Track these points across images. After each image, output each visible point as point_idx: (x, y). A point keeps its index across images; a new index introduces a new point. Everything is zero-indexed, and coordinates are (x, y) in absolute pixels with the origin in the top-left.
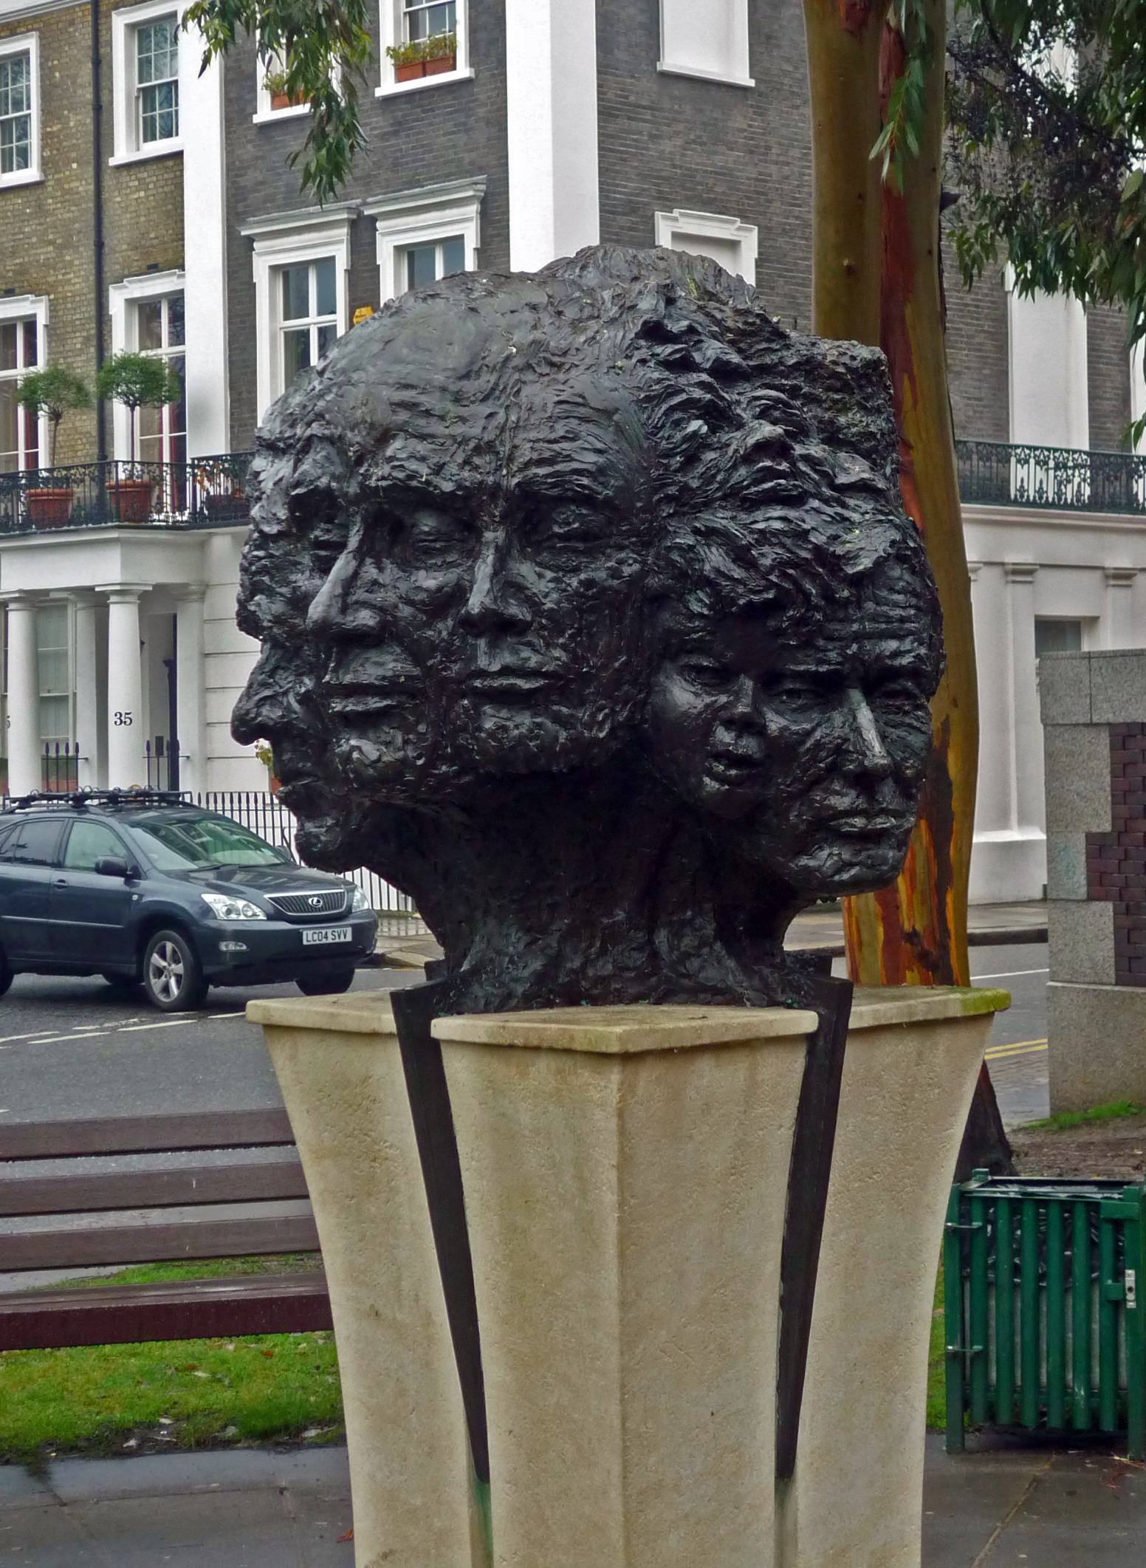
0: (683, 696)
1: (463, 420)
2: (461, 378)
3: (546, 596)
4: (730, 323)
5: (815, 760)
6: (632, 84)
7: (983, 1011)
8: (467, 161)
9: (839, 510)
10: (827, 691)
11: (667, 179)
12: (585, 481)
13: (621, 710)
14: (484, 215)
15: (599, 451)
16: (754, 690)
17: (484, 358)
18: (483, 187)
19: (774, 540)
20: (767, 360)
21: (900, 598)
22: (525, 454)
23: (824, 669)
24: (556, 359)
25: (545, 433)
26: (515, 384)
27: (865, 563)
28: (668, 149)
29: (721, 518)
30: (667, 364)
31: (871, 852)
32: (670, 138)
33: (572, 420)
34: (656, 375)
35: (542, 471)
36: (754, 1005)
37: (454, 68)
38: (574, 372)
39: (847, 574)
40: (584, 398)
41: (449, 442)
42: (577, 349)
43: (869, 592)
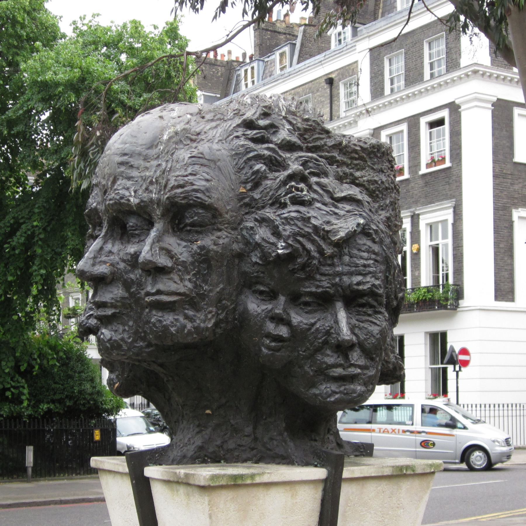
0: (255, 306)
1: (147, 168)
2: (148, 148)
3: (181, 254)
4: (299, 125)
5: (316, 338)
6: (505, 167)
7: (428, 471)
8: (449, 194)
9: (333, 209)
10: (324, 301)
11: (516, 198)
12: (199, 195)
13: (221, 313)
14: (454, 212)
15: (207, 180)
16: (285, 301)
17: (160, 138)
18: (454, 203)
19: (292, 223)
20: (318, 143)
21: (365, 255)
22: (172, 183)
23: (320, 290)
24: (194, 137)
25: (183, 173)
26: (172, 150)
27: (342, 234)
28: (517, 188)
29: (269, 213)
30: (255, 140)
31: (347, 387)
32: (517, 184)
33: (196, 166)
34: (242, 143)
35: (179, 190)
36: (298, 465)
37: (445, 163)
38: (202, 142)
39: (332, 241)
40: (203, 154)
41: (140, 179)
42: (205, 132)
43: (346, 251)
